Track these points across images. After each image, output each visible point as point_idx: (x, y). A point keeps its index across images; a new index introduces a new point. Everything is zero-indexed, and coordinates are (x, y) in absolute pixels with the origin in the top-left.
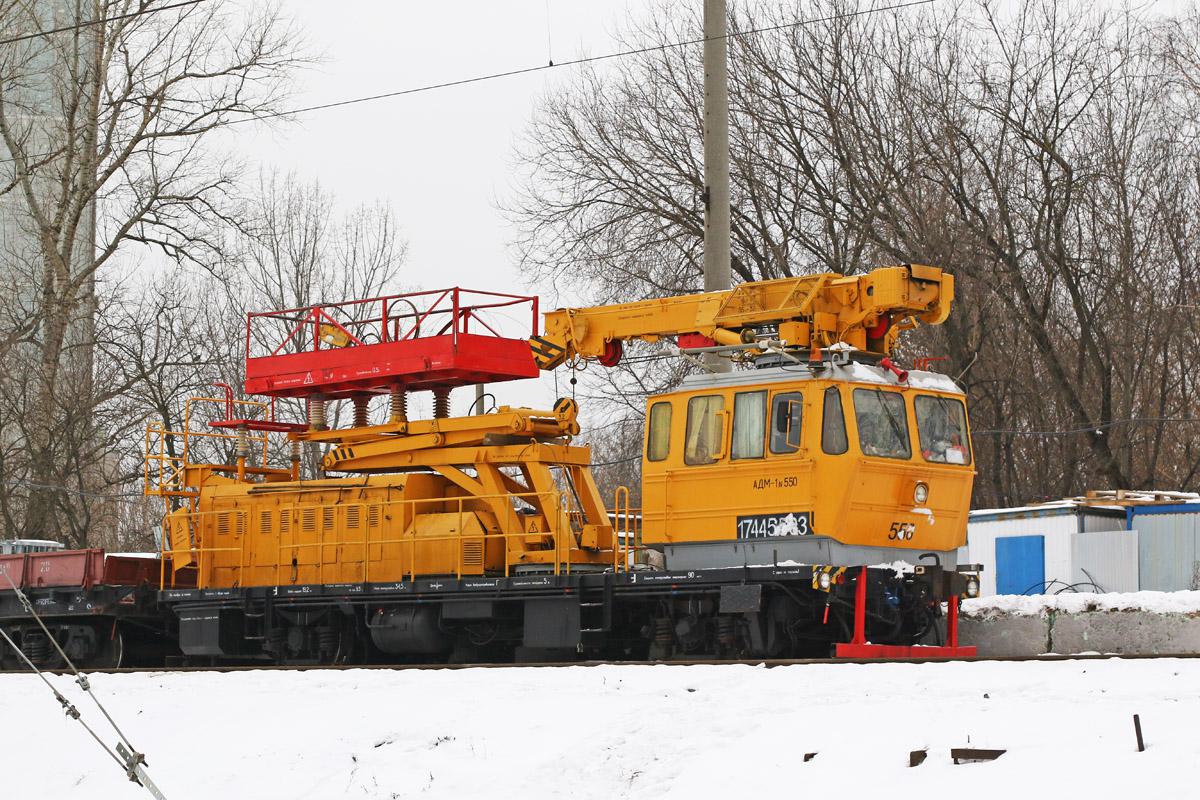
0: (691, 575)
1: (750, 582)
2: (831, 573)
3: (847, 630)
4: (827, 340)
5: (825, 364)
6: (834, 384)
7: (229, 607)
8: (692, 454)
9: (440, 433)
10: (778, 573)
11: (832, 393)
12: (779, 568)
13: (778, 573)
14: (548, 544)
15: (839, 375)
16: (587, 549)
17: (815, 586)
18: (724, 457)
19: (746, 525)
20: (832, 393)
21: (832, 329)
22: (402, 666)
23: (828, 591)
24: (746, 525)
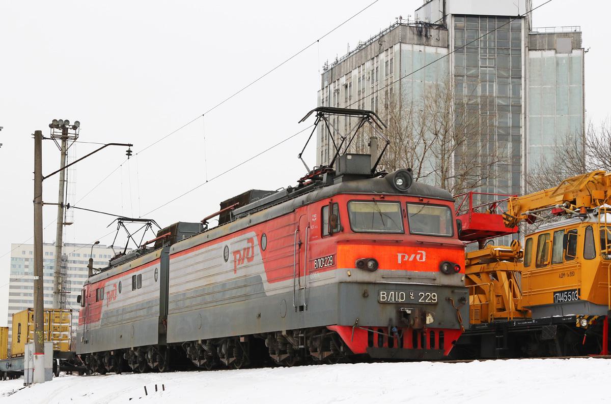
0: (534, 321)
1: (554, 324)
2: (588, 320)
3: (600, 346)
4: (598, 204)
5: (587, 215)
6: (590, 224)
7: (531, 330)
8: (539, 263)
9: (468, 259)
10: (564, 319)
11: (589, 228)
12: (564, 317)
13: (564, 319)
14: (503, 309)
15: (593, 220)
16: (520, 311)
17: (578, 326)
18: (549, 263)
19: (557, 296)
20: (589, 228)
21: (602, 198)
22: (468, 360)
23: (586, 328)
24: (557, 296)
